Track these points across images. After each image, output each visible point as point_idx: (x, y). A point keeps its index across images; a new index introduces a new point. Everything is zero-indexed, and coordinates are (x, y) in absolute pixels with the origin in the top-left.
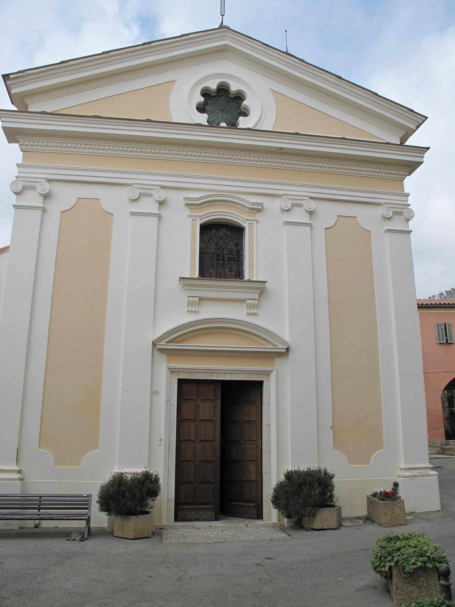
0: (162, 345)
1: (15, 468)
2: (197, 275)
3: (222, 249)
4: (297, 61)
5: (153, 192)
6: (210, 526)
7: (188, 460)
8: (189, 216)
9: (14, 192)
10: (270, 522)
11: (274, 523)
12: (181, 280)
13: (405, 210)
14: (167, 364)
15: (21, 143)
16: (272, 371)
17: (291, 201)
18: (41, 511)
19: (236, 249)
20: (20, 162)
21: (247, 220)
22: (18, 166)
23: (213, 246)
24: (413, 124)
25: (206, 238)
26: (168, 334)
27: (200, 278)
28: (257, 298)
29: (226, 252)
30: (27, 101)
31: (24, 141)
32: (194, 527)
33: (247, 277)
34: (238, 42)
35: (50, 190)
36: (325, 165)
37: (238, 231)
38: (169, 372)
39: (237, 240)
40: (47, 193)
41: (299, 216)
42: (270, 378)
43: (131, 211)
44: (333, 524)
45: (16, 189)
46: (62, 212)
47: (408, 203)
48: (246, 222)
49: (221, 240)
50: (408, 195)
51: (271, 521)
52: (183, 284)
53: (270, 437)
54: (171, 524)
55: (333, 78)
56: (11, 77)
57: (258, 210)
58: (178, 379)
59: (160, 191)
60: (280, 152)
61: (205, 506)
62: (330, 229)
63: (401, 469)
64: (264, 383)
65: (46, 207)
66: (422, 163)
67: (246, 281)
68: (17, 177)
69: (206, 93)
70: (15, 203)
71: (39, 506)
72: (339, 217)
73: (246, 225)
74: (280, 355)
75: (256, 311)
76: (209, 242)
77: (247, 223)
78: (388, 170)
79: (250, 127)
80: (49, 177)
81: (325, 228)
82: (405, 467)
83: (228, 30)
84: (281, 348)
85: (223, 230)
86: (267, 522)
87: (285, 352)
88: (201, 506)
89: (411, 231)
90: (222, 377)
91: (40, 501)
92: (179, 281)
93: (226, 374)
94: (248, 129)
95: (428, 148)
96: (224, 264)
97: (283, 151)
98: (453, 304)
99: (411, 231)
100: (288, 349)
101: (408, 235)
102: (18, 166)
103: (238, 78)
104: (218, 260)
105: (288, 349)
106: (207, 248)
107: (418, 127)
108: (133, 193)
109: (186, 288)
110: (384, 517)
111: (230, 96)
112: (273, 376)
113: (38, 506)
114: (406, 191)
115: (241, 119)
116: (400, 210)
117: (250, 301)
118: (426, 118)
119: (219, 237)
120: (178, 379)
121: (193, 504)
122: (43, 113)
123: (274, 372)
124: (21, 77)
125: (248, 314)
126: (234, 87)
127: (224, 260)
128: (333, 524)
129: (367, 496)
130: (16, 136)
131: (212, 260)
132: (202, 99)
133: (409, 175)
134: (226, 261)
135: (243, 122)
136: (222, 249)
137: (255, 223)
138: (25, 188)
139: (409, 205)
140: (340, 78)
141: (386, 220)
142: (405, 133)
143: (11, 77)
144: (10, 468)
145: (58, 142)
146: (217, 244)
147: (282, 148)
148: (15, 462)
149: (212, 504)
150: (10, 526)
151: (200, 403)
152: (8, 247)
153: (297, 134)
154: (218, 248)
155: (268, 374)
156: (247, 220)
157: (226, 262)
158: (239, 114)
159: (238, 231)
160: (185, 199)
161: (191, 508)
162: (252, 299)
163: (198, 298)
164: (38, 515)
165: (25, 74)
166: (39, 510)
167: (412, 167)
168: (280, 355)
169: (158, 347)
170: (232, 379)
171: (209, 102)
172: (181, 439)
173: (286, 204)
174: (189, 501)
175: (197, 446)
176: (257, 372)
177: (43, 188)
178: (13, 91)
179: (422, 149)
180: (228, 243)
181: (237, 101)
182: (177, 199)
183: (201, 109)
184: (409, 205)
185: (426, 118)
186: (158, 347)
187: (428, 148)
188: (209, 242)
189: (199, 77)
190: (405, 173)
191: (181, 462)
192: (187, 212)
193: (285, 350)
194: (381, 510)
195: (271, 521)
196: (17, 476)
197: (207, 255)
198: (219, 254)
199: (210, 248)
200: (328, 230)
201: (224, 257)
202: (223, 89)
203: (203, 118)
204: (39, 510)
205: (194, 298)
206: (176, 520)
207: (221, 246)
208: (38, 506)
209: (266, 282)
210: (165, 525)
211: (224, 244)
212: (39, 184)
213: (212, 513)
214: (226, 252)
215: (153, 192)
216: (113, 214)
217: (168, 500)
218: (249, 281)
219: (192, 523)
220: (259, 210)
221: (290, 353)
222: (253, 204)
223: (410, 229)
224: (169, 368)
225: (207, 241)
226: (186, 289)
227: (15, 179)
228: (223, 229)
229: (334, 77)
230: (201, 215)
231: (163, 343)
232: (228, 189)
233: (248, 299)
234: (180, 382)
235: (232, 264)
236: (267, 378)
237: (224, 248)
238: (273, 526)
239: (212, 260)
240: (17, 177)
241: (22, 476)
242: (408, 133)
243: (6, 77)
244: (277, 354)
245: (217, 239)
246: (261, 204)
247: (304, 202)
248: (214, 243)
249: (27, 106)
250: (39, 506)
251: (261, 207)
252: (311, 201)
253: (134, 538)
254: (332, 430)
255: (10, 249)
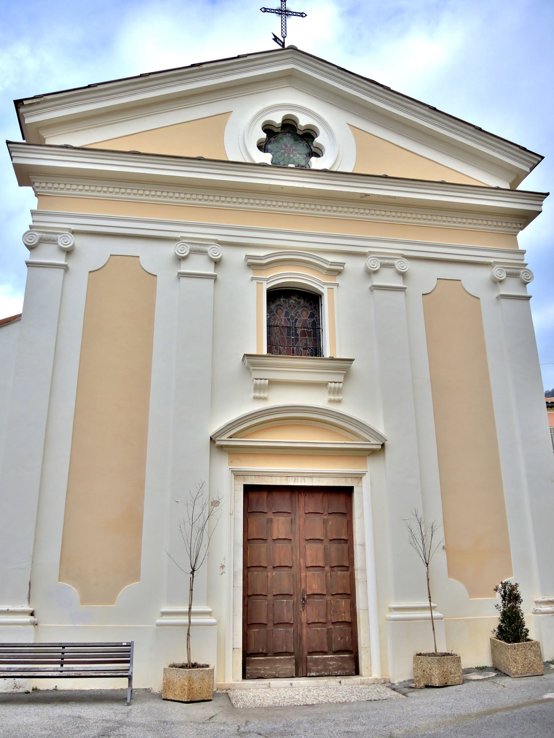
0: (224, 440)
1: (27, 608)
2: (265, 352)
3: (295, 318)
4: (381, 88)
5: (208, 249)
6: (291, 684)
7: (258, 593)
8: (253, 279)
9: (26, 245)
10: (370, 678)
11: (376, 679)
12: (246, 357)
13: (522, 271)
14: (229, 465)
15: (37, 184)
16: (365, 474)
17: (379, 261)
18: (65, 666)
19: (311, 320)
20: (35, 208)
21: (325, 284)
22: (33, 213)
23: (283, 317)
24: (527, 166)
25: (273, 307)
26: (231, 426)
27: (271, 355)
28: (342, 381)
29: (298, 325)
30: (44, 134)
31: (40, 183)
32: (269, 686)
33: (327, 353)
34: (308, 66)
35: (73, 245)
36: (419, 216)
37: (312, 299)
38: (233, 477)
39: (312, 310)
40: (70, 247)
41: (387, 278)
42: (362, 483)
43: (179, 271)
44: (458, 678)
45: (30, 241)
46: (90, 272)
47: (525, 262)
48: (324, 286)
49: (292, 309)
50: (523, 252)
51: (371, 676)
52: (248, 362)
53: (365, 561)
54: (238, 682)
55: (426, 110)
56: (25, 102)
57: (336, 272)
58: (244, 485)
59: (216, 247)
60: (364, 200)
61: (282, 657)
62: (427, 296)
63: (536, 602)
64: (355, 490)
65: (69, 266)
66: (540, 212)
67: (327, 359)
68: (31, 227)
69: (268, 128)
70: (29, 260)
71: (62, 659)
72: (439, 281)
73: (324, 290)
74: (373, 453)
75: (340, 397)
76: (276, 312)
77: (326, 287)
78: (497, 222)
79: (328, 167)
80: (73, 227)
81: (423, 294)
82: (543, 600)
83: (294, 51)
84: (374, 444)
85: (294, 298)
86: (367, 678)
87: (380, 450)
88: (277, 658)
89: (529, 298)
90: (301, 482)
91: (63, 653)
92: (243, 359)
93: (306, 478)
94: (325, 171)
95: (547, 194)
96: (297, 340)
97: (367, 198)
98: (552, 403)
99: (529, 298)
100: (383, 445)
101: (527, 301)
102: (33, 213)
103: (308, 111)
104: (289, 334)
105: (383, 445)
106: (275, 319)
107: (532, 169)
108: (182, 249)
109: (252, 368)
110: (514, 664)
111: (298, 132)
112: (366, 480)
113: (60, 660)
114: (521, 247)
115: (313, 159)
116: (515, 271)
117: (333, 385)
118: (543, 158)
119: (290, 306)
120: (244, 485)
121: (265, 655)
122: (66, 147)
123: (368, 475)
124: (38, 103)
125: (331, 401)
126: (303, 121)
127: (297, 335)
128: (458, 678)
129: (491, 639)
130: (30, 176)
131: (282, 334)
132: (264, 135)
133: (522, 229)
134: (299, 335)
135: (315, 163)
136: (295, 318)
137: (335, 288)
138: (42, 241)
139: (526, 265)
140: (435, 109)
141: (499, 283)
142: (515, 177)
143: (25, 102)
144: (19, 608)
145: (84, 184)
146: (287, 314)
147: (367, 195)
148: (27, 600)
149: (291, 654)
150: (21, 689)
151: (273, 517)
152: (20, 316)
153: (386, 177)
154: (289, 320)
155: (359, 477)
156: (325, 284)
157: (299, 337)
158: (309, 155)
159: (312, 299)
160: (248, 257)
161: (263, 660)
162: (335, 382)
163: (267, 381)
164: (61, 671)
165: (42, 99)
166: (62, 665)
167: (526, 218)
168: (373, 453)
169: (218, 443)
170: (314, 485)
171: (272, 139)
172: (248, 565)
173: (374, 264)
174: (261, 651)
175: (269, 574)
176: (345, 476)
177: (66, 240)
178: (27, 121)
179: (540, 195)
180: (302, 313)
181: (306, 139)
182: (238, 257)
183: (262, 147)
184: (526, 265)
185: (543, 158)
186: (218, 443)
187: (547, 194)
188: (276, 312)
189: (259, 108)
190: (519, 226)
191: (249, 596)
192: (251, 274)
193: (380, 447)
194: (509, 656)
195: (371, 676)
196: (29, 619)
197: (275, 328)
198: (289, 327)
199: (278, 320)
200: (425, 296)
201: (296, 330)
202: (289, 125)
203: (267, 158)
204: (62, 665)
205: (263, 381)
206: (244, 677)
207: (292, 318)
208: (60, 660)
209: (352, 360)
210: (231, 684)
211: (296, 315)
212: (60, 236)
213: (291, 667)
214: (298, 325)
215: (208, 249)
216: (156, 276)
217: (233, 648)
218: (332, 359)
219: (266, 681)
220: (339, 272)
221: (388, 452)
222: (333, 264)
223: (529, 294)
224: (232, 471)
225: (275, 311)
226: (253, 370)
227: (29, 229)
228: (294, 296)
229: (427, 108)
230: (268, 277)
231: (225, 438)
232: (300, 246)
233: (331, 382)
234: (248, 489)
235: (306, 339)
236: (358, 483)
237: (296, 320)
238: (376, 682)
239: (282, 334)
240: (31, 227)
241: (36, 620)
242: (521, 176)
243: (18, 103)
244: (369, 452)
245: (287, 308)
246: (342, 264)
247: (396, 262)
248: (284, 313)
249: (44, 140)
250: (62, 659)
251: (341, 268)
252: (405, 260)
253: (189, 700)
254: (444, 552)
255: (22, 318)
